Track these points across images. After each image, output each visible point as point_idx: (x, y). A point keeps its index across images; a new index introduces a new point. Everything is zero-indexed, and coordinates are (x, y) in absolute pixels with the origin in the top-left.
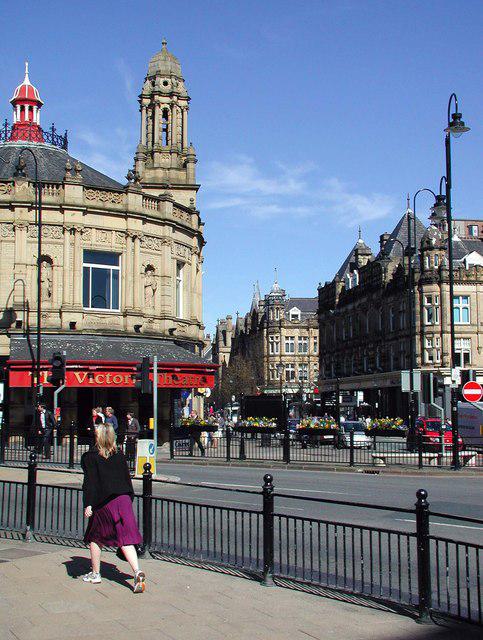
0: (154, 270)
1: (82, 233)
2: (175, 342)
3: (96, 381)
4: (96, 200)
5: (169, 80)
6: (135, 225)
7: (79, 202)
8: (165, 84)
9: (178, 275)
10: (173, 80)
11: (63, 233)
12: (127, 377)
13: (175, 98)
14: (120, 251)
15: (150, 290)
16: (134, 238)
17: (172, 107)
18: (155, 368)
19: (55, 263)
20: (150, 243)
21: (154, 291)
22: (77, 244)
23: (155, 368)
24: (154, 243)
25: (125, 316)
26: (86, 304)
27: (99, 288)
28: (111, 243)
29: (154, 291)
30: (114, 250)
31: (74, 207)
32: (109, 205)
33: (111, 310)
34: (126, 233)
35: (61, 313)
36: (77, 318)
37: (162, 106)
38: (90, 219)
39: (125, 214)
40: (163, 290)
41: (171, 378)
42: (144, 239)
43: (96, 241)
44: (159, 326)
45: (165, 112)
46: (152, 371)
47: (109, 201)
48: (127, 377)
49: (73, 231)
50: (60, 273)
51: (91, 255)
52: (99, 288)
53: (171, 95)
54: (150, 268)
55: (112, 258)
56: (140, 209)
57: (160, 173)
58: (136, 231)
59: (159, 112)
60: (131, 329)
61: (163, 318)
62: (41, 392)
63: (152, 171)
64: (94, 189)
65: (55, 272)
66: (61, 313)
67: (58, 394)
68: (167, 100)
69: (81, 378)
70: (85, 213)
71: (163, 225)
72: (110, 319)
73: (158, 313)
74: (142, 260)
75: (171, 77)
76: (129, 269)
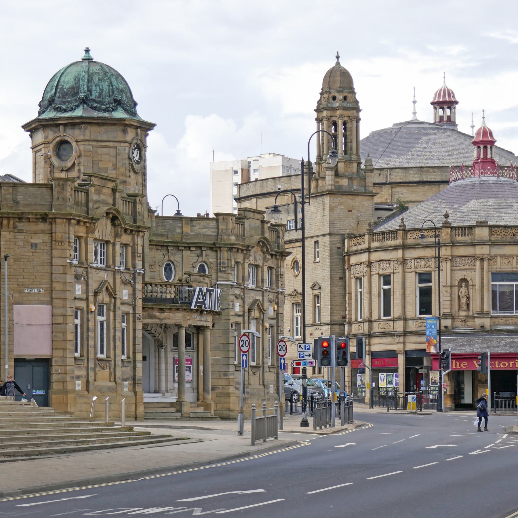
16: (482, 260)
31: (482, 243)
38: (496, 250)
58: (482, 255)
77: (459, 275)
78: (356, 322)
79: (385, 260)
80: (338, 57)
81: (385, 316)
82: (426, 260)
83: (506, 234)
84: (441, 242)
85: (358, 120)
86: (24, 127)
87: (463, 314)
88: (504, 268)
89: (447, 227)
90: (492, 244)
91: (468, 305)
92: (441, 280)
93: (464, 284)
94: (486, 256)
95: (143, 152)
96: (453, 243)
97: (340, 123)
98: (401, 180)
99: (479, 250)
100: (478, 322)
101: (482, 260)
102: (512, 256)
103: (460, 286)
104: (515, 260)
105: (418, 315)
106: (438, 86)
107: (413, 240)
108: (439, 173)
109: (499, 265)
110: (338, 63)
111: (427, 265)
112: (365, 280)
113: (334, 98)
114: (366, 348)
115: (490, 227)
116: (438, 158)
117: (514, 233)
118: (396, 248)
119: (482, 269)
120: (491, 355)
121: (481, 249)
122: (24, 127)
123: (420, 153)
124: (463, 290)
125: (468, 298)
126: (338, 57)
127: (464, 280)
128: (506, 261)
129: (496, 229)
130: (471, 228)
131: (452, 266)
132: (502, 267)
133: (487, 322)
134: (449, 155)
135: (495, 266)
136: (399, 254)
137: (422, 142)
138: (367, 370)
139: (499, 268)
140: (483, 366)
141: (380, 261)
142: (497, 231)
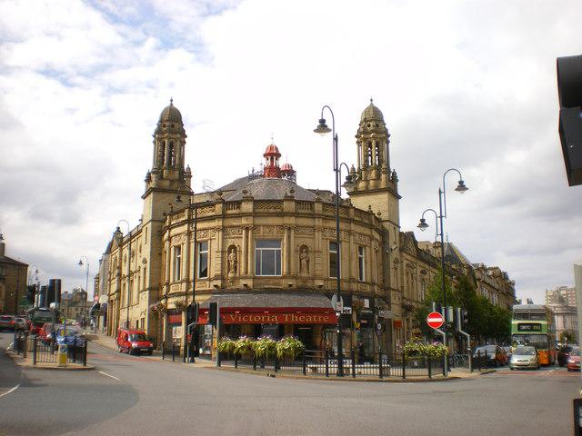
6: (291, 221)
7: (251, 211)
9: (361, 254)
15: (304, 261)
16: (289, 229)
26: (258, 273)
31: (319, 216)
32: (272, 211)
34: (282, 227)
39: (282, 214)
54: (304, 247)
77: (230, 242)
78: (174, 283)
85: (388, 142)
87: (231, 275)
89: (220, 203)
90: (296, 215)
91: (236, 267)
93: (304, 250)
95: (159, 159)
97: (373, 144)
99: (244, 221)
100: (243, 282)
101: (289, 229)
102: (273, 226)
103: (230, 252)
104: (275, 229)
106: (269, 143)
109: (261, 234)
110: (372, 104)
112: (184, 248)
113: (369, 126)
115: (296, 201)
118: (182, 223)
119: (247, 237)
124: (232, 254)
125: (236, 262)
127: (233, 247)
128: (267, 230)
130: (280, 202)
131: (223, 235)
133: (250, 283)
136: (218, 223)
138: (183, 323)
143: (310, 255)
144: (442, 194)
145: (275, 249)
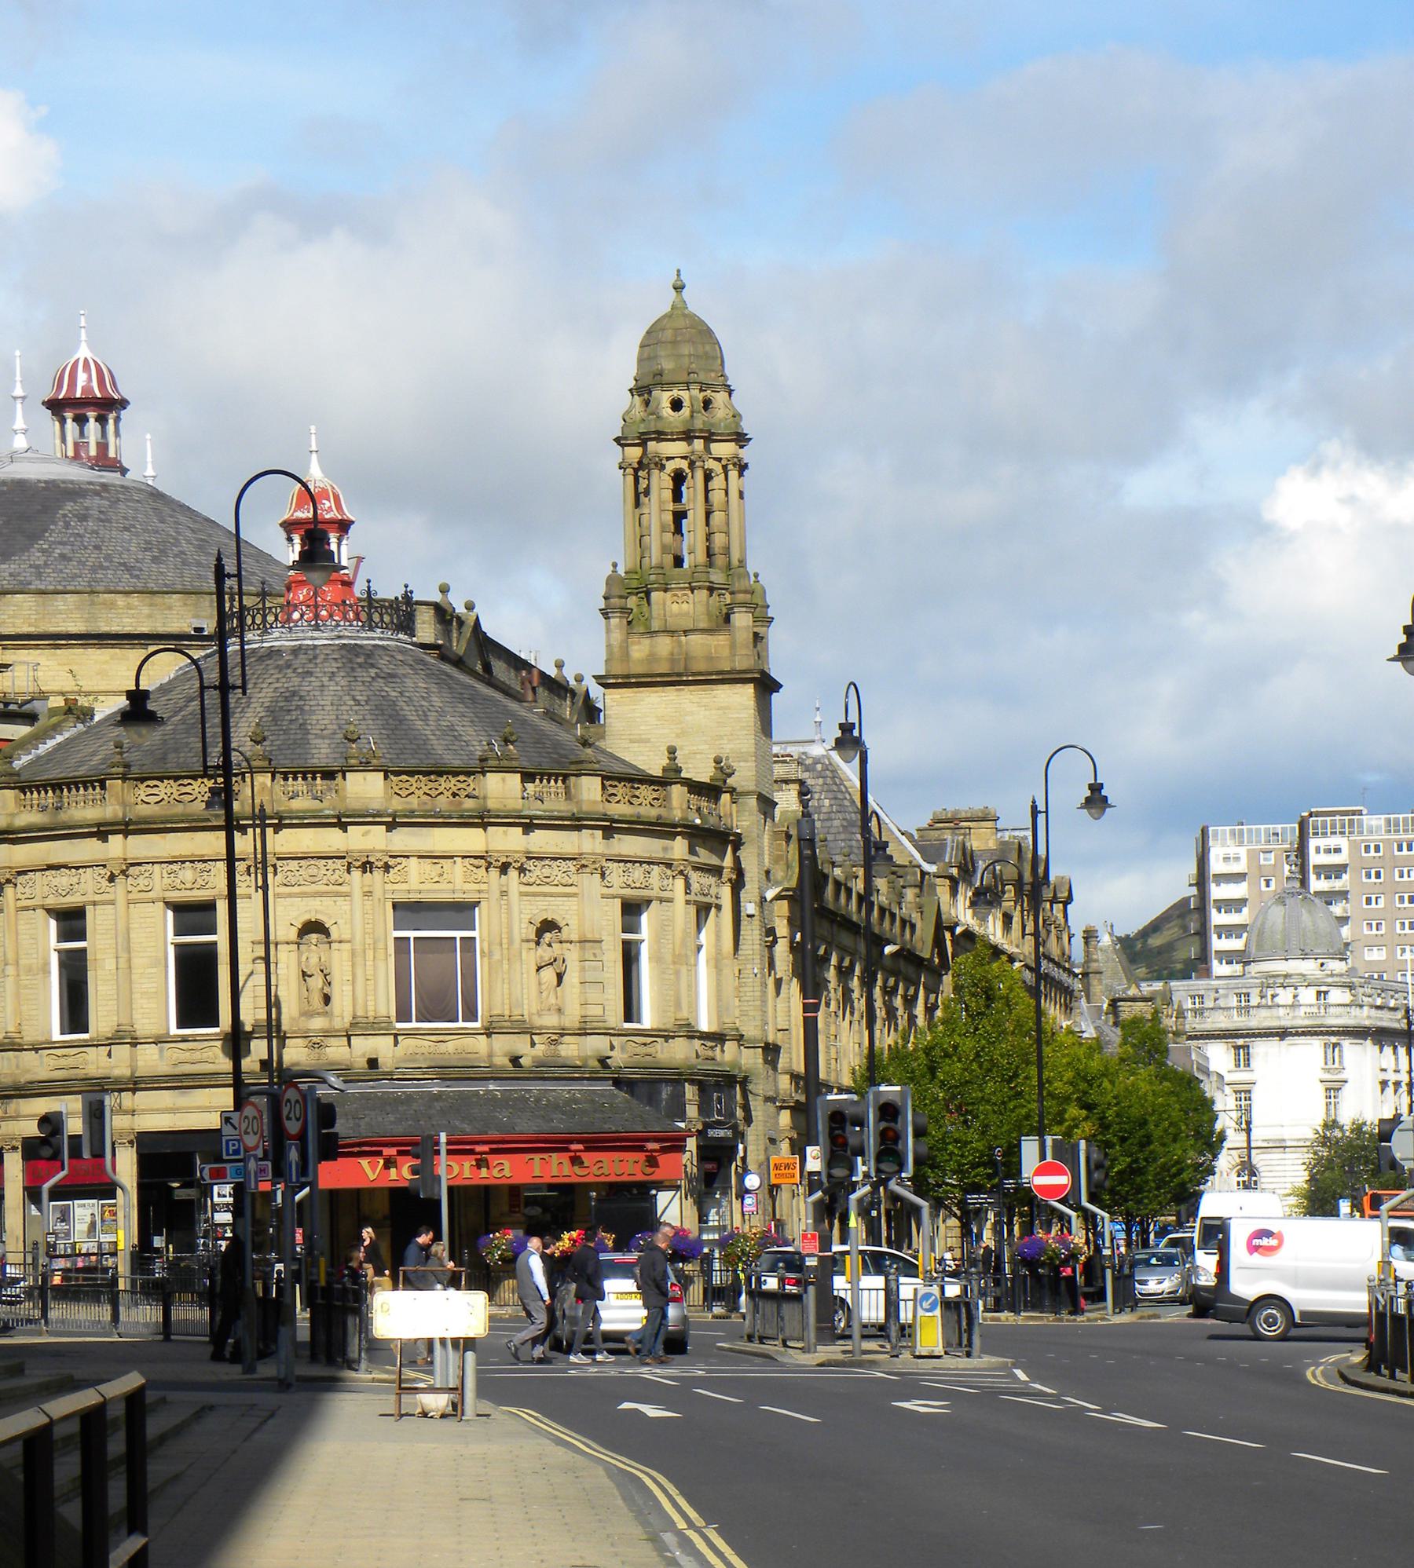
0: (560, 929)
1: (387, 868)
2: (617, 1082)
3: (504, 1170)
4: (417, 794)
5: (685, 396)
6: (509, 841)
8: (677, 405)
10: (695, 392)
11: (349, 872)
12: (467, 1165)
13: (699, 444)
14: (471, 897)
15: (549, 975)
17: (692, 465)
18: (443, 1150)
19: (334, 935)
20: (546, 871)
21: (560, 977)
22: (378, 893)
23: (443, 1150)
24: (556, 870)
25: (489, 1035)
26: (403, 1015)
27: (435, 990)
28: (456, 883)
29: (560, 977)
30: (459, 897)
32: (443, 803)
33: (460, 1024)
34: (483, 859)
35: (349, 1037)
36: (381, 1047)
37: (670, 466)
38: (404, 839)
39: (482, 820)
40: (583, 970)
41: (566, 1163)
42: (529, 865)
43: (417, 881)
44: (572, 1049)
45: (679, 478)
46: (438, 1152)
47: (443, 794)
48: (467, 1165)
49: (367, 866)
50: (346, 956)
51: (408, 911)
52: (435, 990)
53: (688, 436)
54: (548, 926)
55: (462, 911)
56: (515, 803)
57: (664, 645)
59: (661, 483)
60: (502, 1061)
61: (583, 1031)
62: (279, 1200)
63: (646, 642)
64: (411, 774)
65: (335, 955)
66: (349, 1037)
67: (1070, 1218)
68: (679, 448)
69: (374, 1171)
70: (391, 826)
71: (579, 828)
72: (465, 1043)
73: (571, 1019)
74: (527, 912)
75: (688, 385)
76: (503, 917)
79: (65, 867)
80: (679, 288)
81: (180, 1026)
82: (200, 866)
83: (433, 793)
84: (268, 811)
86: (43, 403)
88: (428, 891)
92: (241, 925)
94: (379, 855)
96: (281, 818)
98: (31, 630)
105: (174, 1030)
107: (156, 808)
108: (146, 611)
111: (200, 882)
114: (117, 1123)
116: (124, 565)
117: (454, 789)
120: (448, 1143)
121: (365, 834)
122: (43, 403)
123: (67, 550)
126: (679, 288)
129: (404, 777)
132: (422, 887)
134: (155, 560)
135: (404, 886)
137: (65, 516)
139: (415, 891)
140: (426, 1172)
141: (50, 867)
142: (406, 785)
143: (572, 955)
144: (1041, 818)
145: (458, 934)
